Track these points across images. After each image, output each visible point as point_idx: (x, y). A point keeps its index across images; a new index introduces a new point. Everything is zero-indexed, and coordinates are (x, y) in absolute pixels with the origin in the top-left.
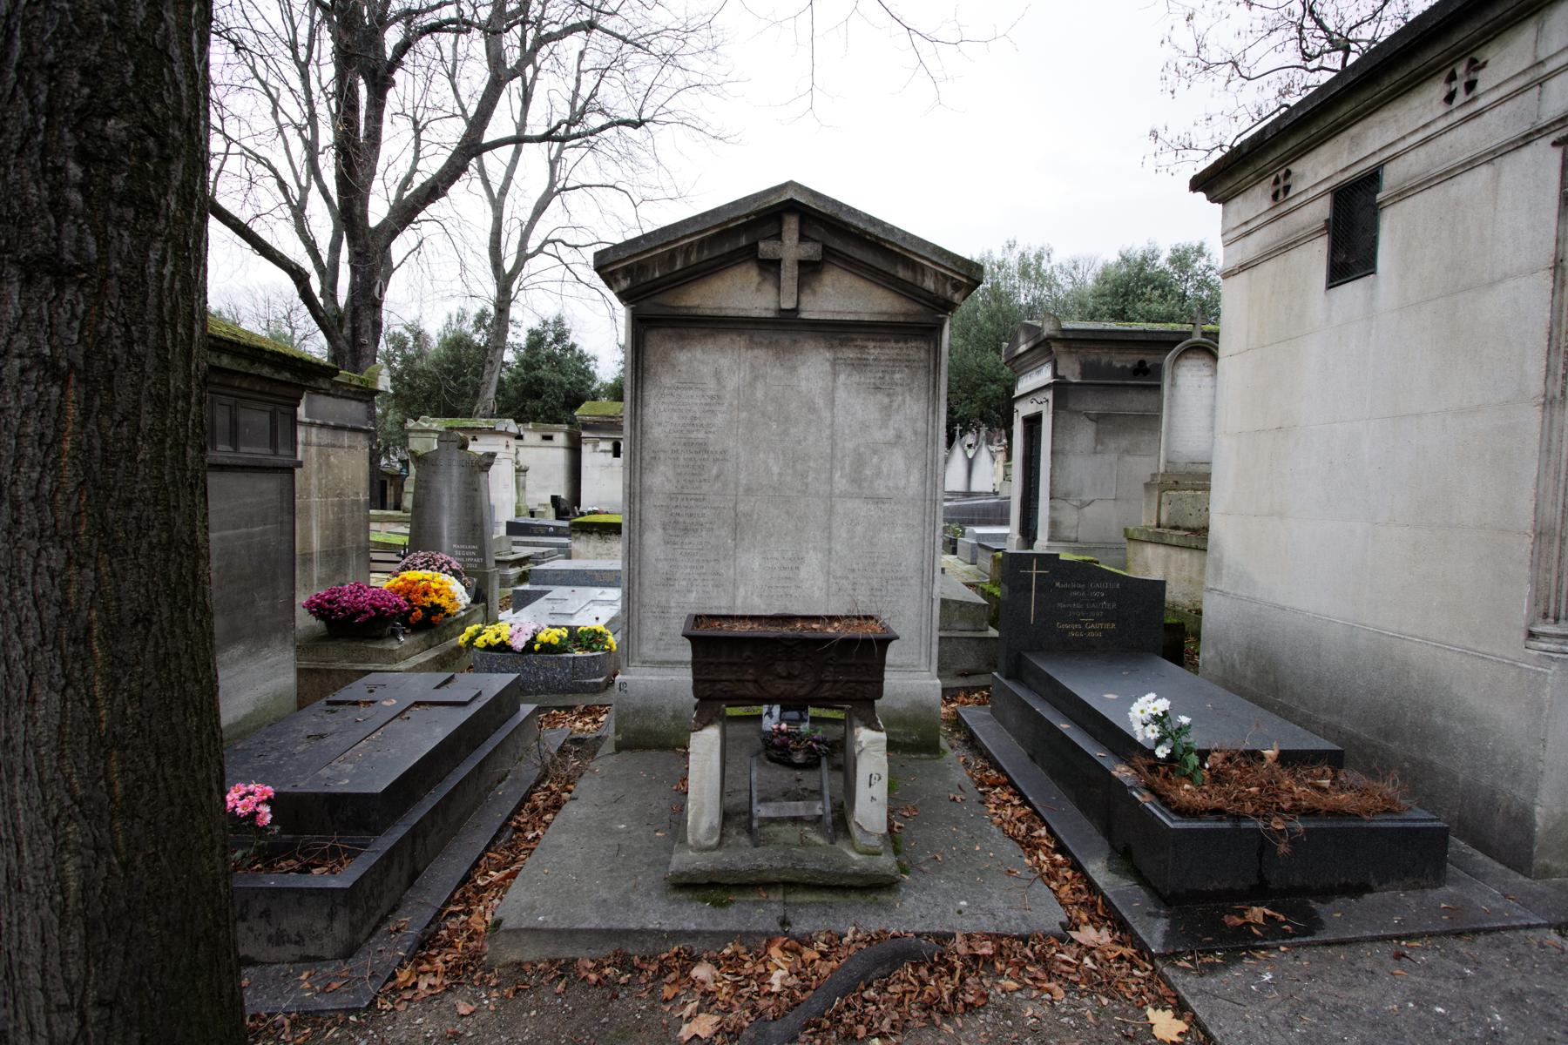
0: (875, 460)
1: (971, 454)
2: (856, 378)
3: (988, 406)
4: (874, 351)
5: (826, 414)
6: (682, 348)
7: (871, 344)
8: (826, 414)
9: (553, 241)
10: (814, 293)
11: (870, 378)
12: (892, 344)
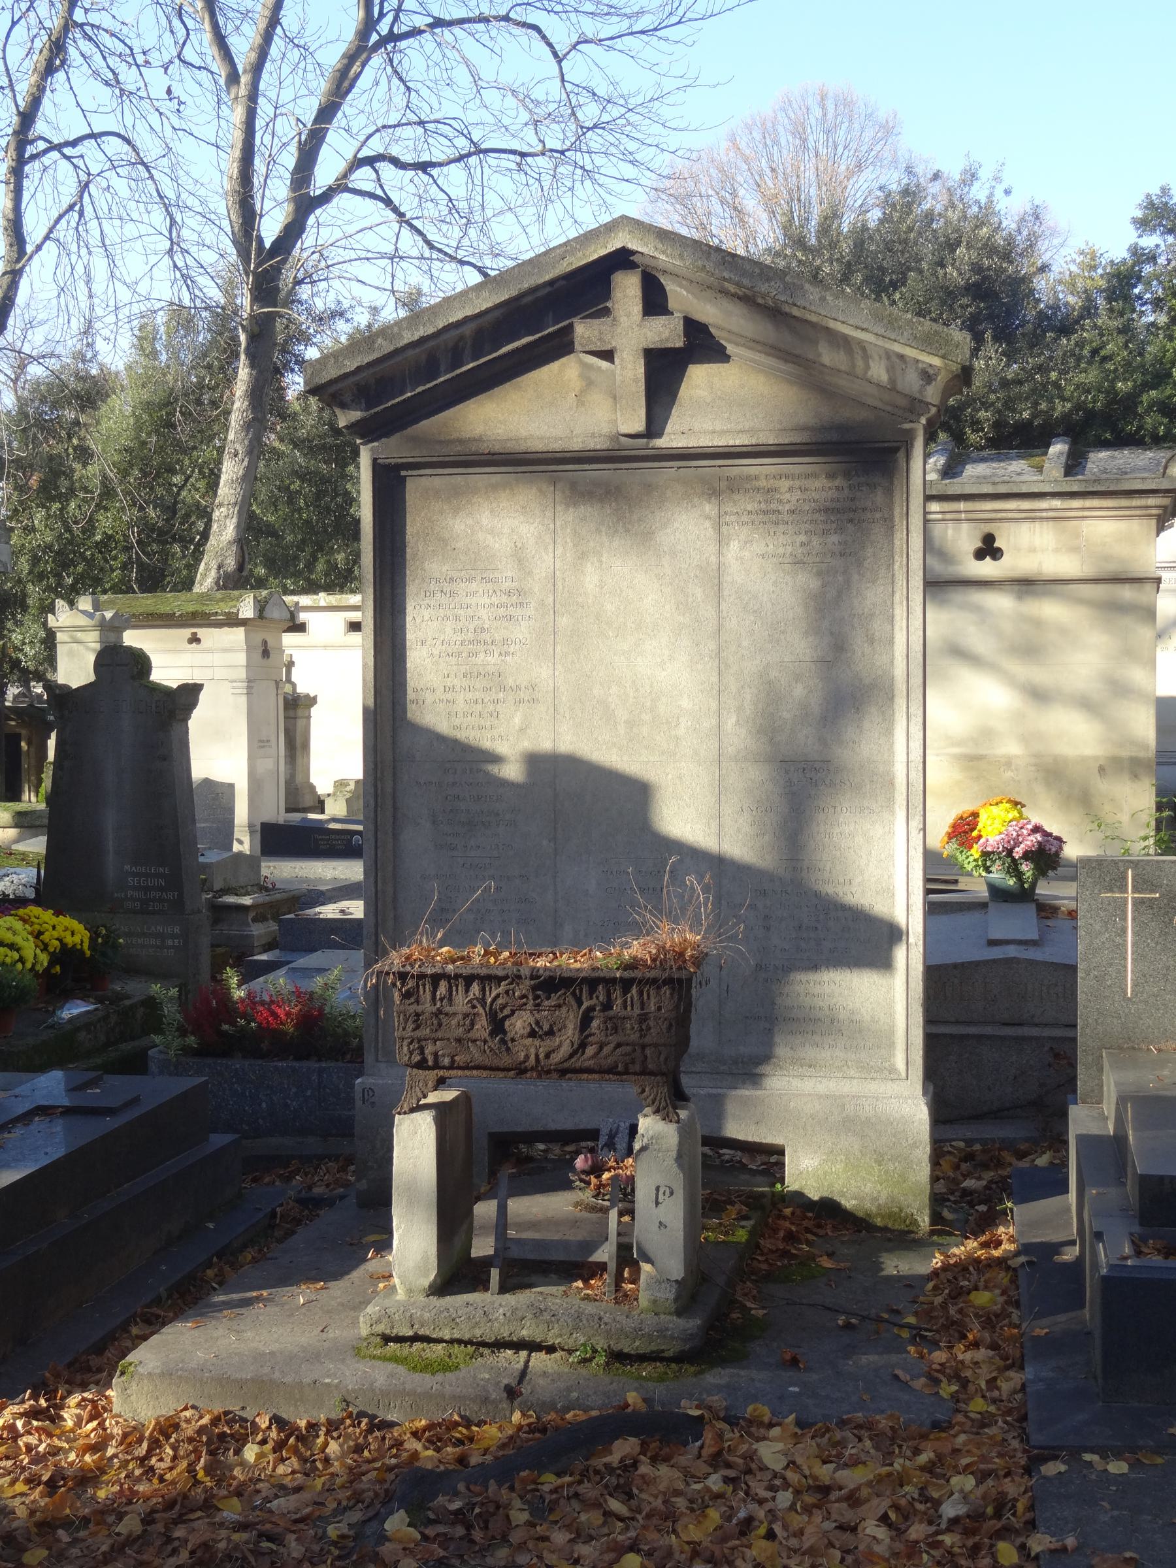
6: (456, 511)
9: (370, 161)
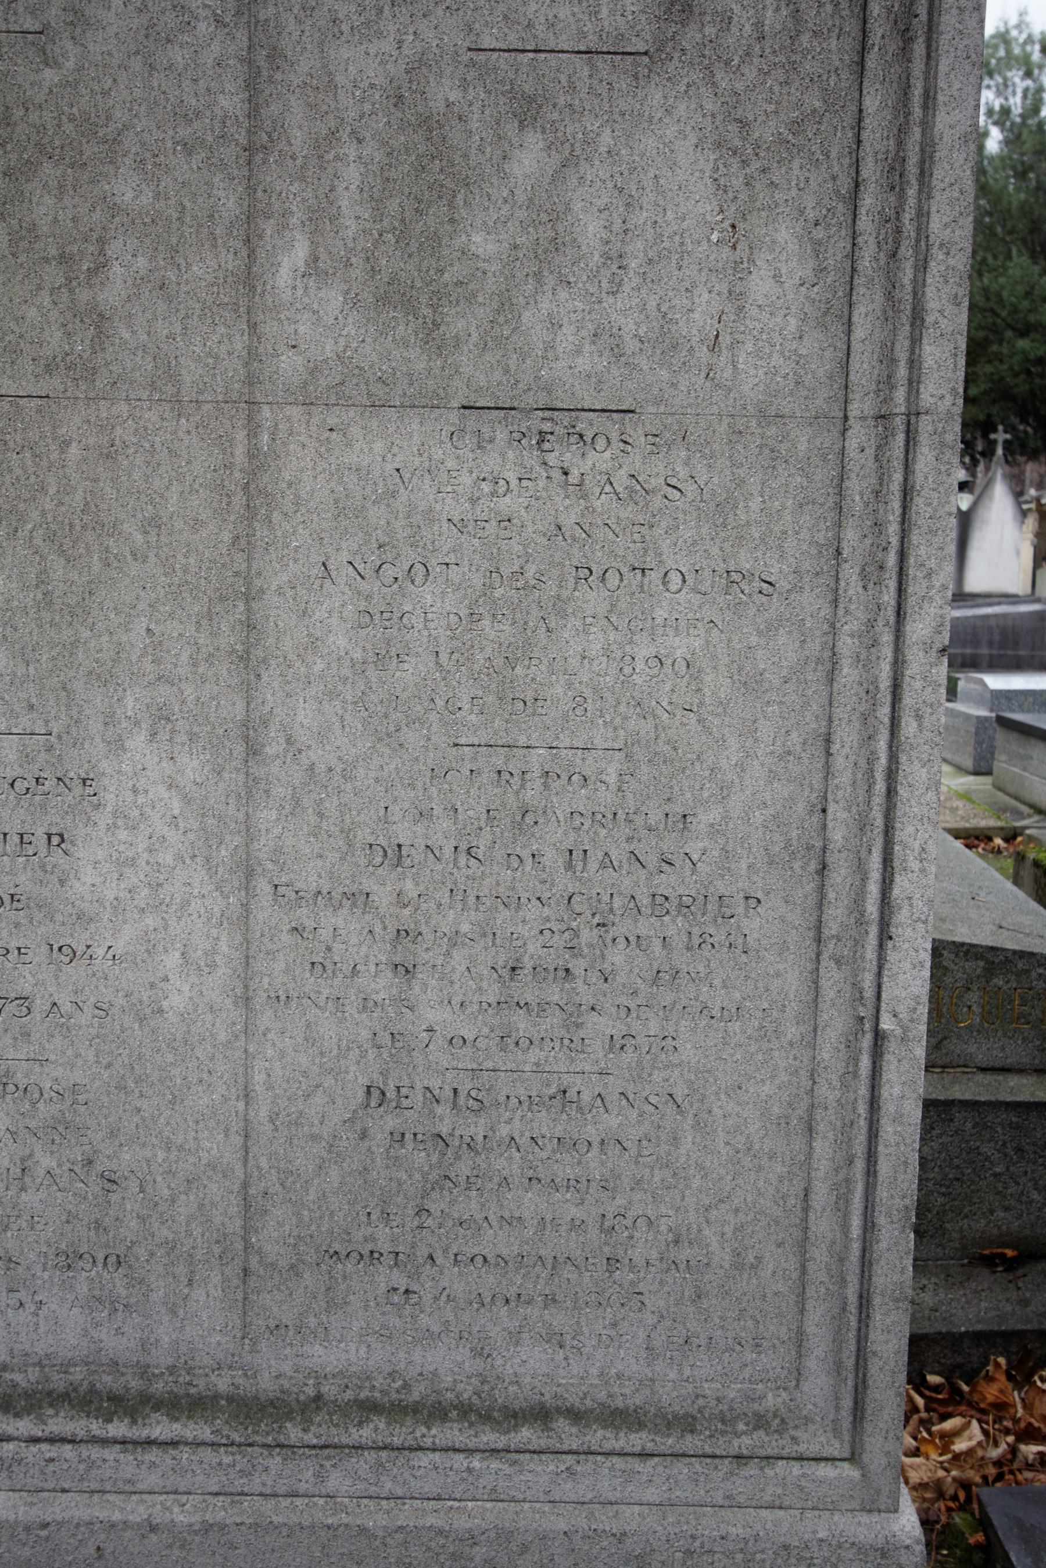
0: (529, 159)
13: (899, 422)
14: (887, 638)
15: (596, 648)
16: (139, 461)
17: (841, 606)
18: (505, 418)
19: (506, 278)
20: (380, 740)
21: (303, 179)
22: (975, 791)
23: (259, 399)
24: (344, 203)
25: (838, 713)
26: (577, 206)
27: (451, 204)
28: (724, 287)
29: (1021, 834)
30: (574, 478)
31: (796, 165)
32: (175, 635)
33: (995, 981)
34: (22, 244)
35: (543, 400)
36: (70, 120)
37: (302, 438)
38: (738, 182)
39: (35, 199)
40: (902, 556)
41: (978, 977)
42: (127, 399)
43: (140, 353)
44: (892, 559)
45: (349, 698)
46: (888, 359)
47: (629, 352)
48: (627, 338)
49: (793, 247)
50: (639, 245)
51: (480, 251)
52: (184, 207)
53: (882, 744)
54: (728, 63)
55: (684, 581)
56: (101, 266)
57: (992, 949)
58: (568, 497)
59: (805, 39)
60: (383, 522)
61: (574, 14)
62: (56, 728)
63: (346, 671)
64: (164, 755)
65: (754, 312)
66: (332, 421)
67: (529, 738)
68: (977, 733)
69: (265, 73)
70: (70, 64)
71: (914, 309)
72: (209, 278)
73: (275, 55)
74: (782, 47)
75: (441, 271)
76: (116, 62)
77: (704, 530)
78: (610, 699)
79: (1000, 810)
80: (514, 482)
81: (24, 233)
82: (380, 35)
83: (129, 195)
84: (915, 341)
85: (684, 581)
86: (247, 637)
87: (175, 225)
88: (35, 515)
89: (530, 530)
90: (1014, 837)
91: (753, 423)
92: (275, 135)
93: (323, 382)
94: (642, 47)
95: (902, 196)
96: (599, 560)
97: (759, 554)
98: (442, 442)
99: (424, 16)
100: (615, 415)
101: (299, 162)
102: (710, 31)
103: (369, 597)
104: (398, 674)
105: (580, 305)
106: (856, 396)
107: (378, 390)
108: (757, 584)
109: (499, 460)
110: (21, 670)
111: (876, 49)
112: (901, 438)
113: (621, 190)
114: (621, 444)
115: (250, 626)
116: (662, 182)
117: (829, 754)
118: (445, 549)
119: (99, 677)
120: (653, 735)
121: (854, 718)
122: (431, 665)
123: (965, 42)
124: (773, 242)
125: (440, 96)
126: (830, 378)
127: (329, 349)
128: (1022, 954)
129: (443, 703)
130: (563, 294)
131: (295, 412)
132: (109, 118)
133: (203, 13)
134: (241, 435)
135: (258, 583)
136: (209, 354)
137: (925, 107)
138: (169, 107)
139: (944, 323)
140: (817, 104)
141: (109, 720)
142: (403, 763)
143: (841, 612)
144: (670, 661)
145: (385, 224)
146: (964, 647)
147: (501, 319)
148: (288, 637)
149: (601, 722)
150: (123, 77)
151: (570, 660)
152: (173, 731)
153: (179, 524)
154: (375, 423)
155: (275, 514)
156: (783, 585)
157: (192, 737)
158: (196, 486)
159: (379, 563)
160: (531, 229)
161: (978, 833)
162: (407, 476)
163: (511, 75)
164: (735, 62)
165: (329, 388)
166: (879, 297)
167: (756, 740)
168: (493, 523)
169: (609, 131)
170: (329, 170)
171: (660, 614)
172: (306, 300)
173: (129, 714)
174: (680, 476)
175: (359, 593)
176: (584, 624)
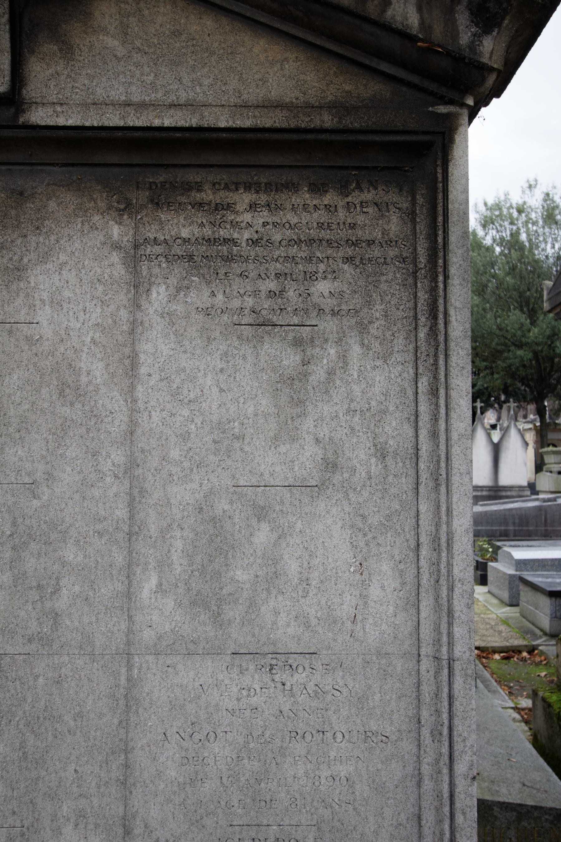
0: (263, 535)
1: (496, 436)
2: (199, 296)
3: (513, 376)
4: (249, 218)
5: (112, 401)
7: (243, 199)
8: (112, 401)
10: (68, 51)
11: (240, 294)
12: (305, 197)
13: (445, 663)
14: (445, 771)
15: (301, 773)
16: (73, 684)
17: (422, 749)
18: (254, 658)
19: (253, 591)
20: (193, 824)
21: (155, 547)
22: (511, 618)
23: (133, 652)
24: (175, 558)
25: (424, 804)
26: (286, 557)
27: (226, 557)
28: (357, 593)
29: (537, 649)
30: (288, 687)
31: (389, 535)
32: (89, 772)
33: (523, 823)
34: (19, 581)
35: (271, 649)
36: (45, 523)
37: (154, 671)
38: (362, 544)
39: (26, 560)
40: (450, 729)
41: (514, 821)
42: (68, 654)
43: (75, 632)
44: (445, 731)
45: (177, 802)
46: (437, 629)
47: (313, 625)
48: (312, 618)
49: (389, 573)
50: (316, 574)
51: (240, 579)
52: (98, 562)
53: (447, 827)
54: (355, 490)
55: (344, 737)
56: (57, 590)
57: (520, 805)
58: (285, 696)
59: (390, 478)
60: (194, 711)
61: (282, 470)
62: (26, 823)
63: (175, 789)
64: (82, 836)
65: (373, 604)
66: (169, 662)
67: (268, 821)
68: (509, 584)
69: (137, 499)
70: (45, 498)
71: (448, 609)
72: (110, 595)
73: (142, 492)
74: (380, 482)
75: (221, 589)
76: (67, 496)
77: (352, 711)
78: (309, 799)
79: (525, 632)
80: (258, 690)
81: (20, 576)
82: (191, 480)
83: (72, 556)
84: (450, 624)
85: (344, 737)
86: (126, 772)
87: (93, 571)
88: (20, 713)
89: (267, 713)
90: (533, 650)
91: (374, 658)
92: (142, 527)
93: (164, 644)
94: (314, 483)
95: (439, 554)
96: (301, 727)
97: (380, 722)
98: (222, 671)
99: (212, 472)
100: (307, 656)
101: (153, 539)
102: (346, 475)
103: (187, 750)
104: (202, 789)
105: (288, 603)
106: (423, 645)
107: (191, 647)
108: (380, 737)
109: (251, 679)
110: (10, 794)
111: (424, 484)
112: (446, 671)
113: (307, 549)
114: (311, 670)
115: (127, 766)
116: (326, 544)
117: (420, 826)
118: (225, 724)
119: (49, 795)
120: (331, 817)
121: (432, 808)
122: (219, 784)
123: (464, 488)
124: (380, 571)
125: (220, 508)
126: (411, 635)
127: (167, 627)
128: (536, 808)
129: (224, 804)
130: (280, 598)
131: (150, 658)
132: (63, 521)
133: (108, 473)
134: (124, 670)
135: (131, 744)
136: (109, 631)
137: (448, 515)
138: (92, 516)
139: (463, 617)
140: (398, 507)
141: (54, 818)
142: (204, 836)
143: (422, 752)
144: (338, 779)
145: (194, 567)
146: (500, 526)
147: (251, 611)
148: (146, 772)
149: (304, 811)
150: (70, 503)
151: (288, 779)
152: (86, 823)
153: (92, 716)
154: (189, 663)
155: (140, 709)
156: (393, 737)
157: (97, 826)
158: (101, 696)
159: (192, 732)
160: (264, 568)
161: (514, 649)
162: (205, 688)
163: (254, 497)
164: (358, 489)
165: (167, 646)
166: (432, 601)
167: (383, 818)
168: (249, 711)
169: (300, 521)
170: (168, 543)
171: (333, 754)
172: (156, 604)
173: (64, 814)
174: (340, 684)
175: (182, 748)
176: (295, 760)
